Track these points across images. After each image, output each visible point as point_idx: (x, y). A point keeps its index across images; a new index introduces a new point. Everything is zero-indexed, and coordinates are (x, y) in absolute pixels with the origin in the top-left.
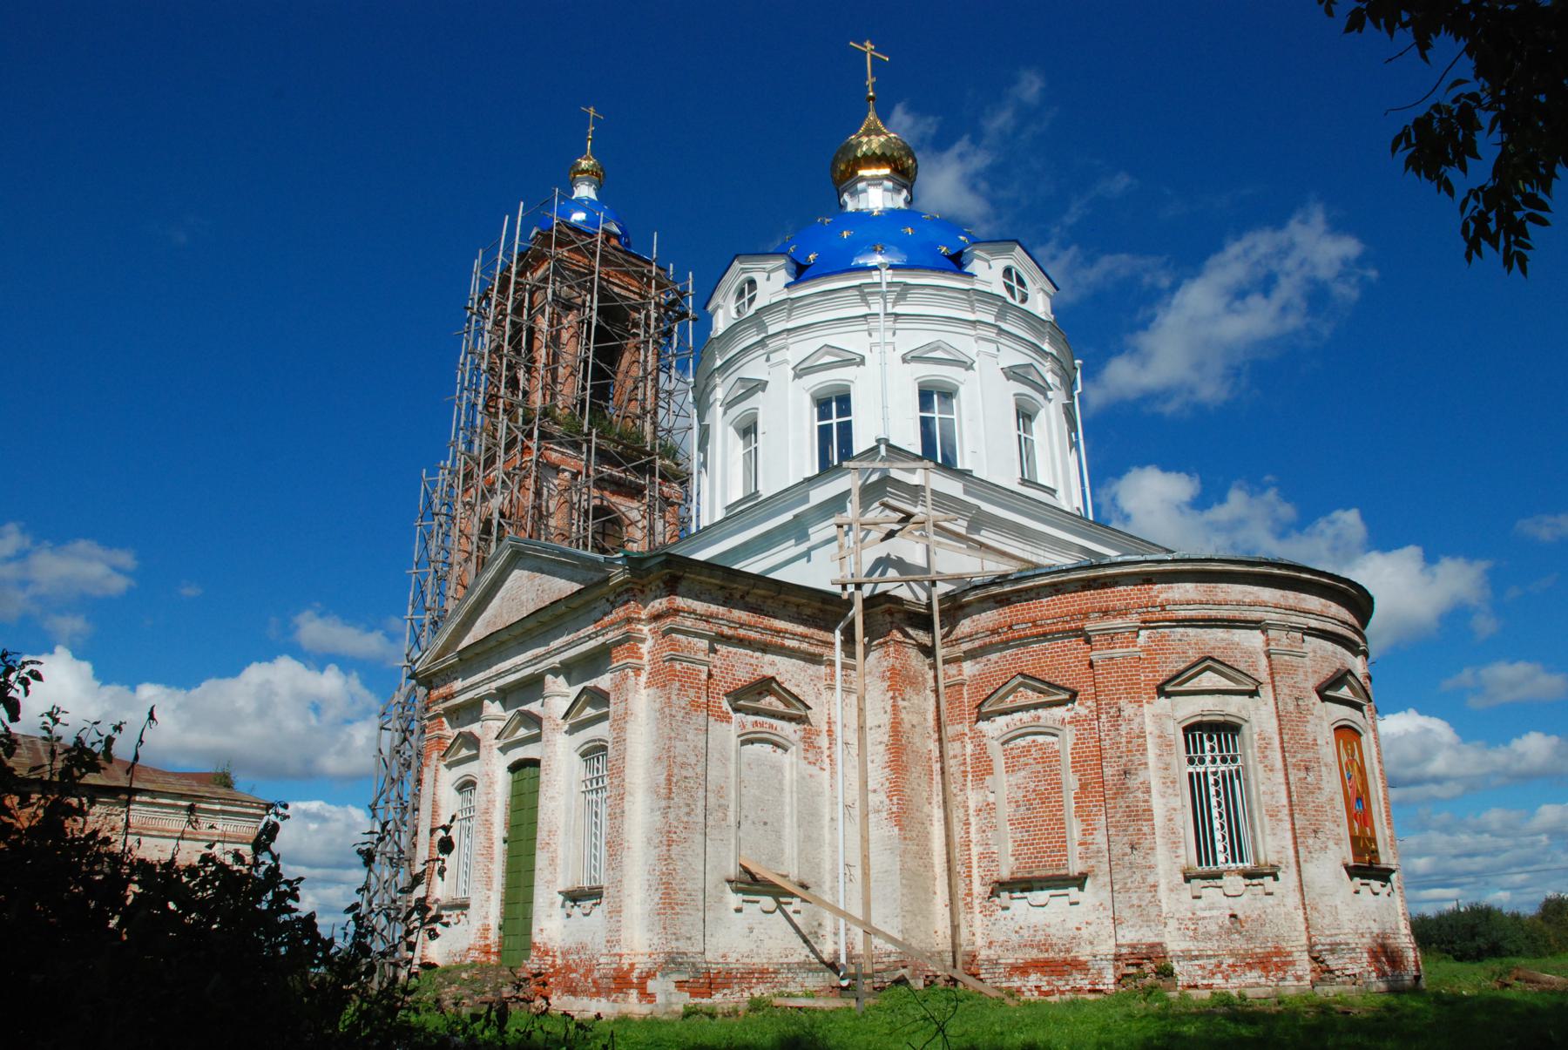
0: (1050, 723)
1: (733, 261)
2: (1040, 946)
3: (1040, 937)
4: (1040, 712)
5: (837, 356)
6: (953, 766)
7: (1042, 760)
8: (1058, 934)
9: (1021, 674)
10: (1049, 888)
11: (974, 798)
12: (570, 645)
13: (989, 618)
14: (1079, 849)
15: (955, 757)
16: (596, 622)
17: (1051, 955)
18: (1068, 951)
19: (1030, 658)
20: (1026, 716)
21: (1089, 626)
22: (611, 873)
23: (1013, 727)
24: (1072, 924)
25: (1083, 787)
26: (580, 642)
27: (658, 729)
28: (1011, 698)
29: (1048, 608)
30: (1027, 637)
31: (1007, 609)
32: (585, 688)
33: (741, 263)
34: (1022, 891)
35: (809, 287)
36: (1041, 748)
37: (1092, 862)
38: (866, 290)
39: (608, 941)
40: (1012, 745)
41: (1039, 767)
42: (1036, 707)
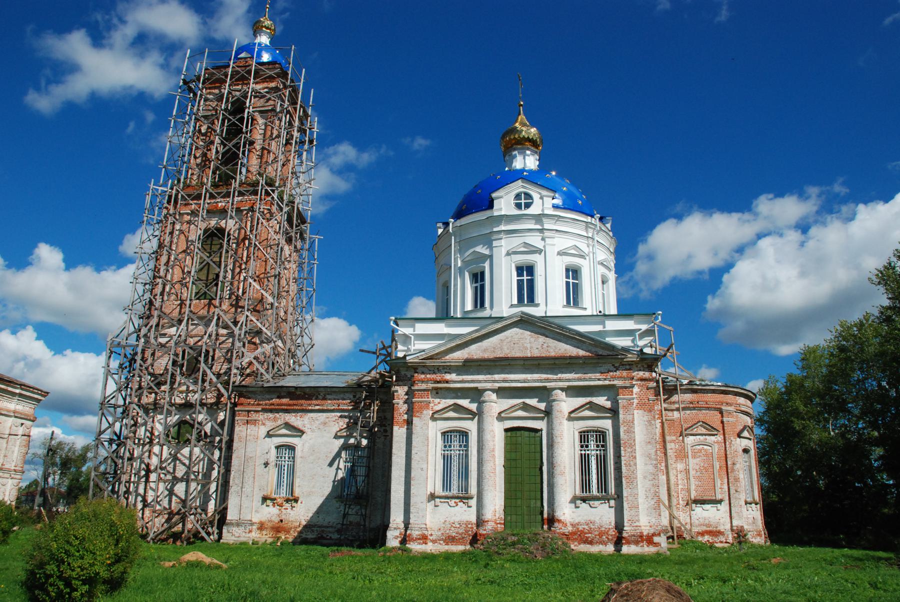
0: (710, 442)
1: (518, 180)
2: (706, 525)
3: (707, 522)
4: (707, 437)
5: (577, 251)
6: (670, 452)
7: (706, 455)
8: (713, 521)
9: (703, 422)
10: (711, 504)
11: (680, 466)
12: (579, 380)
13: (688, 397)
14: (720, 490)
15: (672, 449)
16: (602, 373)
17: (711, 529)
18: (717, 527)
19: (703, 415)
20: (702, 438)
21: (724, 408)
22: (629, 490)
23: (696, 441)
24: (717, 518)
25: (720, 467)
26: (585, 380)
27: (647, 429)
28: (695, 430)
29: (710, 397)
30: (703, 407)
31: (695, 395)
32: (590, 403)
33: (523, 183)
34: (701, 504)
35: (579, 216)
36: (706, 450)
37: (723, 495)
38: (590, 226)
39: (630, 520)
40: (694, 448)
41: (705, 458)
42: (705, 435)
